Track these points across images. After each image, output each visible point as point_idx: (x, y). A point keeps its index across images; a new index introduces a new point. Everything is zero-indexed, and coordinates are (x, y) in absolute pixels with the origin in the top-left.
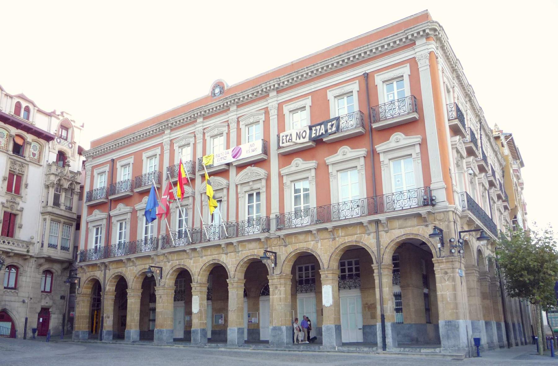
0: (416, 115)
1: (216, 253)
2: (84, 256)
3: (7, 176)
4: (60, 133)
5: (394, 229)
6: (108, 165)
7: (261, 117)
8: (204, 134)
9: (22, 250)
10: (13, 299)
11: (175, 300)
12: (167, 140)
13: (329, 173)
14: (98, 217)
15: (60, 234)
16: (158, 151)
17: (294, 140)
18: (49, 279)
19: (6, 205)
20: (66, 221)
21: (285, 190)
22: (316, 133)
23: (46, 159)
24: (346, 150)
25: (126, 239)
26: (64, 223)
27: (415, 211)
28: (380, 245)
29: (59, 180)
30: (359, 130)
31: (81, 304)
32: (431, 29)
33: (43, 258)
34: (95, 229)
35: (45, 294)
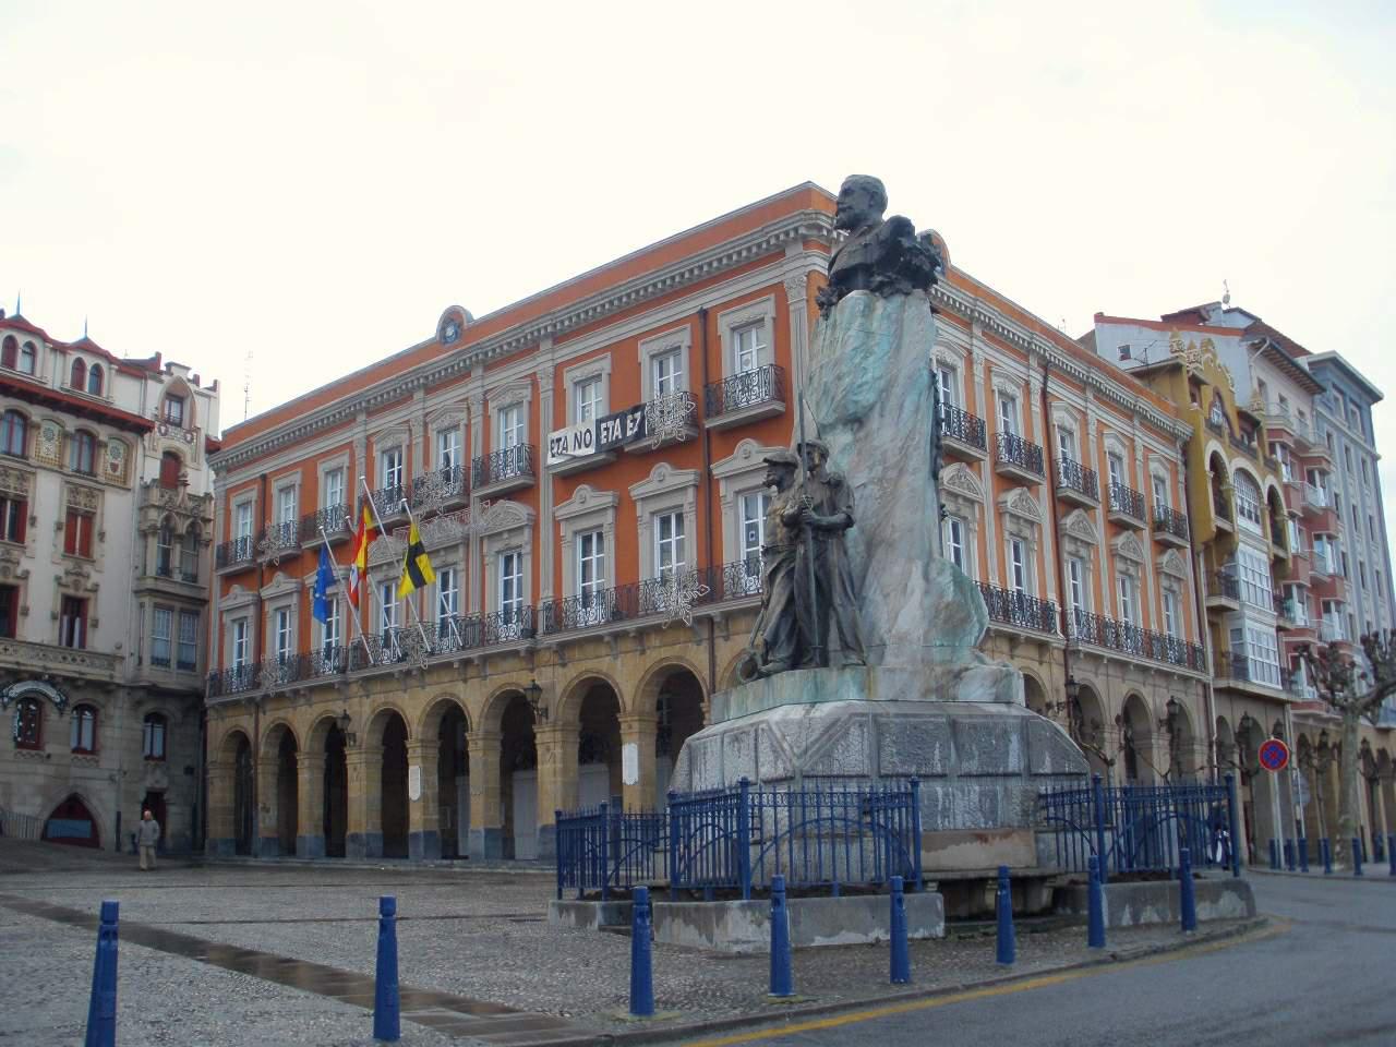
0: (778, 406)
2: (218, 682)
3: (64, 520)
4: (166, 412)
6: (256, 486)
8: (426, 425)
9: (96, 673)
10: (89, 772)
14: (241, 600)
15: (163, 634)
16: (344, 460)
18: (159, 732)
19: (64, 581)
20: (186, 606)
23: (139, 475)
24: (748, 447)
25: (291, 650)
26: (183, 611)
29: (168, 519)
32: (809, 227)
33: (143, 688)
34: (236, 628)
35: (152, 763)
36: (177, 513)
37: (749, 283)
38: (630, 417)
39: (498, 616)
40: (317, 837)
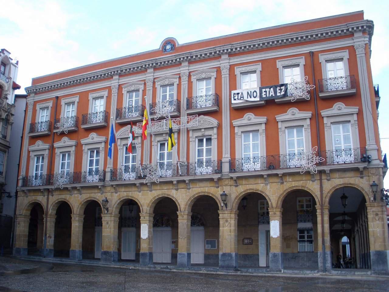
1: (166, 188)
5: (335, 178)
7: (212, 74)
11: (191, 226)
12: (31, 101)
13: (278, 128)
17: (245, 98)
21: (236, 139)
22: (266, 95)
24: (341, 106)
27: (356, 165)
28: (321, 190)
30: (139, 119)
31: (22, 224)
36: (3, 109)
37: (47, 96)
38: (278, 88)
39: (33, 177)
40: (80, 251)
